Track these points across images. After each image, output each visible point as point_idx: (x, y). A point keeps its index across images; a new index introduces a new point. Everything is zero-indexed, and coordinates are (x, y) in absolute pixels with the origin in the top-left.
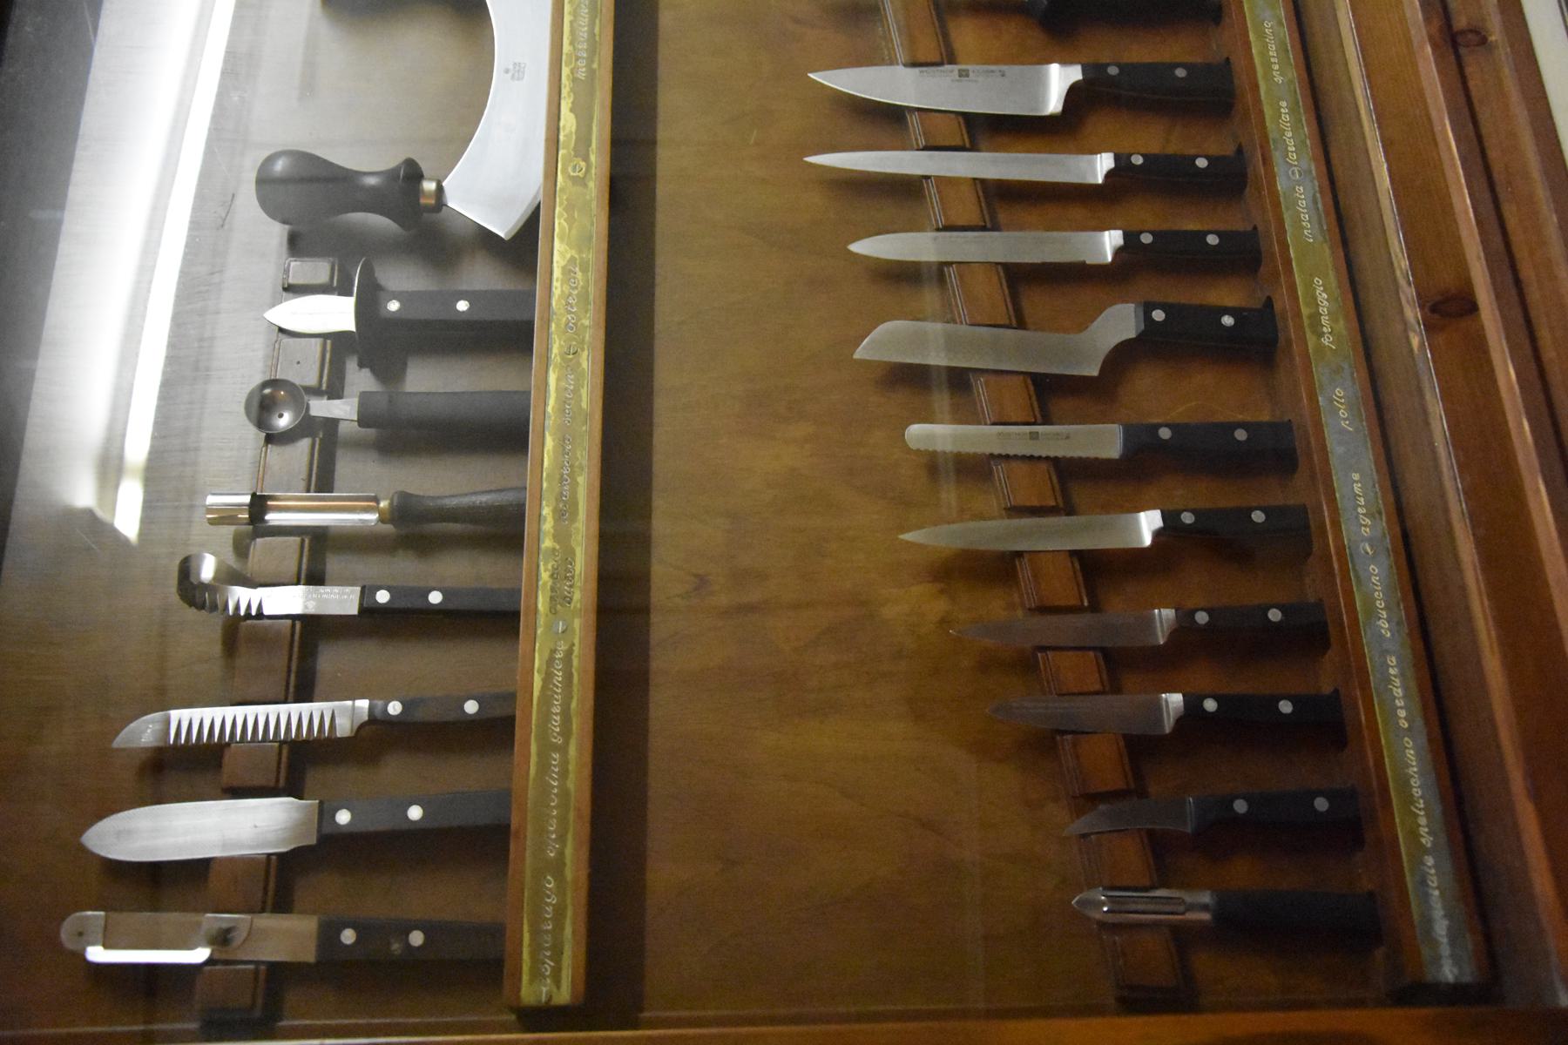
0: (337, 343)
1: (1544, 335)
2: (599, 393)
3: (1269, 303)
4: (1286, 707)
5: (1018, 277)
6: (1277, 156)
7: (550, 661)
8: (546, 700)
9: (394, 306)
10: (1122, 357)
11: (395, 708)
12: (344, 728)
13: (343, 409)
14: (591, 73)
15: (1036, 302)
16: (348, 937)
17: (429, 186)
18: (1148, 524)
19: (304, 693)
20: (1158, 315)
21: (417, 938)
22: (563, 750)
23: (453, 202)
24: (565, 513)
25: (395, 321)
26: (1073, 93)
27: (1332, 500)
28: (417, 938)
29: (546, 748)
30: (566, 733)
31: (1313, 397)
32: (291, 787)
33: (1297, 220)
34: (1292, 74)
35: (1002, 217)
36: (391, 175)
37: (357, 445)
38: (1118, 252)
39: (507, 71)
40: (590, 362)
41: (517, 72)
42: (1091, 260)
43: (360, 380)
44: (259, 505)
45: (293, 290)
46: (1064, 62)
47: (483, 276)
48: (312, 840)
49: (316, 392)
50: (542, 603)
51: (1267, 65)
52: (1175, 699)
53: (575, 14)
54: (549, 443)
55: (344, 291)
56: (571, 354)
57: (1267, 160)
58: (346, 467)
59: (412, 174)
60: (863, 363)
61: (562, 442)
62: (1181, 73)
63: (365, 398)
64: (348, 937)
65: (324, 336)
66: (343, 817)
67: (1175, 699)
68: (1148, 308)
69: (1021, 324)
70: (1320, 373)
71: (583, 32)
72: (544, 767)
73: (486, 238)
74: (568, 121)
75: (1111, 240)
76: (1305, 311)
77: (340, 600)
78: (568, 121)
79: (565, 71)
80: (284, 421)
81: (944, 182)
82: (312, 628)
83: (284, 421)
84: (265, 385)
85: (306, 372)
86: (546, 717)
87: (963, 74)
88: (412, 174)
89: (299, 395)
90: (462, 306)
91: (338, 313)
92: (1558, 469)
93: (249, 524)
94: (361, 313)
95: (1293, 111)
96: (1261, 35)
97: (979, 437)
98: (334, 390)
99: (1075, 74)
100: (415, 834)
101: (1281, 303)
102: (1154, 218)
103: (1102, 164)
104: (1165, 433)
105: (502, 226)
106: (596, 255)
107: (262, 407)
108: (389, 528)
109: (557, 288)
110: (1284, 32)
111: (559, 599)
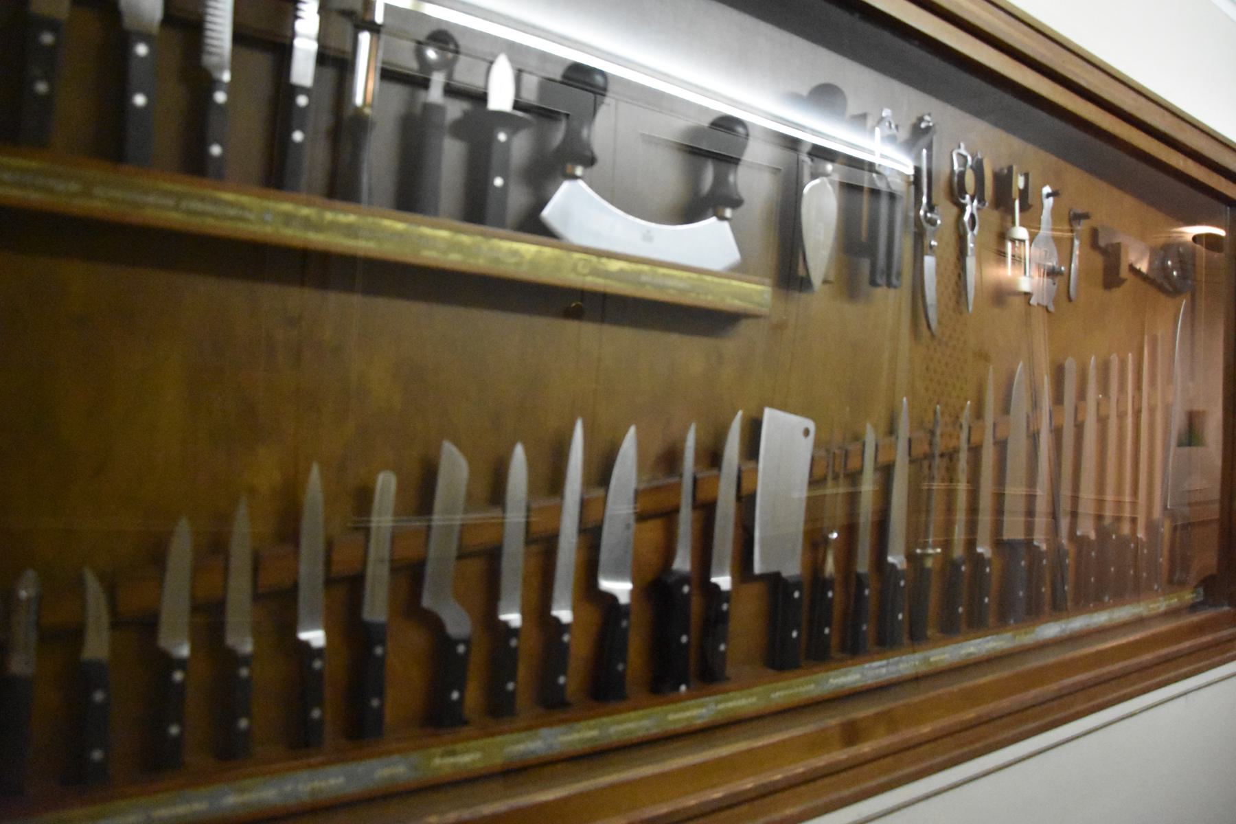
0: (480, 98)
1: (727, 813)
2: (433, 263)
3: (465, 723)
4: (174, 730)
5: (493, 556)
6: (562, 728)
7: (243, 207)
8: (217, 202)
9: (502, 137)
10: (434, 624)
11: (220, 97)
12: (209, 60)
13: (435, 94)
14: (643, 284)
15: (475, 567)
16: (47, 38)
17: (579, 171)
18: (315, 637)
19: (239, 38)
20: (461, 649)
21: (42, 87)
22: (176, 208)
23: (566, 186)
24: (351, 231)
25: (492, 138)
26: (611, 598)
27: (323, 764)
28: (42, 87)
29: (180, 197)
30: (190, 212)
31: (399, 751)
32: (169, 19)
33: (518, 742)
34: (615, 738)
35: (534, 548)
36: (588, 146)
37: (411, 101)
38: (505, 624)
39: (649, 231)
40: (453, 260)
41: (648, 237)
42: (502, 604)
43: (455, 109)
44: (375, 29)
45: (519, 75)
46: (633, 593)
47: (518, 199)
48: (128, 23)
49: (450, 76)
50: (286, 207)
51: (619, 723)
52: (184, 651)
53: (681, 279)
54: (400, 226)
55: (517, 105)
56: (459, 247)
57: (562, 722)
58: (398, 92)
59: (590, 161)
60: (439, 448)
61: (400, 235)
62: (620, 667)
63: (439, 109)
64: (47, 38)
65: (486, 87)
66: (142, 50)
67: (184, 651)
68: (467, 642)
69: (461, 556)
70: (415, 757)
71: (670, 283)
72: (166, 194)
73: (542, 203)
74: (615, 266)
75: (513, 618)
76: (459, 747)
77: (303, 69)
78: (615, 266)
79: (646, 268)
80: (431, 54)
81: (558, 510)
82: (283, 51)
83: (431, 54)
84: (457, 45)
85: (465, 75)
86: (203, 199)
87: (628, 527)
88: (590, 161)
89: (447, 66)
90: (498, 182)
91: (501, 98)
92: (676, 819)
93: (379, 39)
94: (500, 115)
95: (591, 739)
96: (641, 718)
97: (383, 519)
98: (451, 91)
99: (624, 599)
100: (124, 98)
101: (465, 731)
102: (528, 650)
103: (564, 615)
104: (379, 651)
105: (549, 213)
106: (524, 273)
107: (442, 37)
108: (349, 113)
109: (506, 245)
110: (641, 734)
111: (288, 219)
